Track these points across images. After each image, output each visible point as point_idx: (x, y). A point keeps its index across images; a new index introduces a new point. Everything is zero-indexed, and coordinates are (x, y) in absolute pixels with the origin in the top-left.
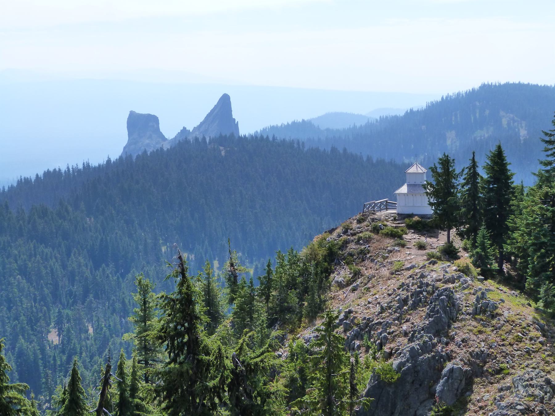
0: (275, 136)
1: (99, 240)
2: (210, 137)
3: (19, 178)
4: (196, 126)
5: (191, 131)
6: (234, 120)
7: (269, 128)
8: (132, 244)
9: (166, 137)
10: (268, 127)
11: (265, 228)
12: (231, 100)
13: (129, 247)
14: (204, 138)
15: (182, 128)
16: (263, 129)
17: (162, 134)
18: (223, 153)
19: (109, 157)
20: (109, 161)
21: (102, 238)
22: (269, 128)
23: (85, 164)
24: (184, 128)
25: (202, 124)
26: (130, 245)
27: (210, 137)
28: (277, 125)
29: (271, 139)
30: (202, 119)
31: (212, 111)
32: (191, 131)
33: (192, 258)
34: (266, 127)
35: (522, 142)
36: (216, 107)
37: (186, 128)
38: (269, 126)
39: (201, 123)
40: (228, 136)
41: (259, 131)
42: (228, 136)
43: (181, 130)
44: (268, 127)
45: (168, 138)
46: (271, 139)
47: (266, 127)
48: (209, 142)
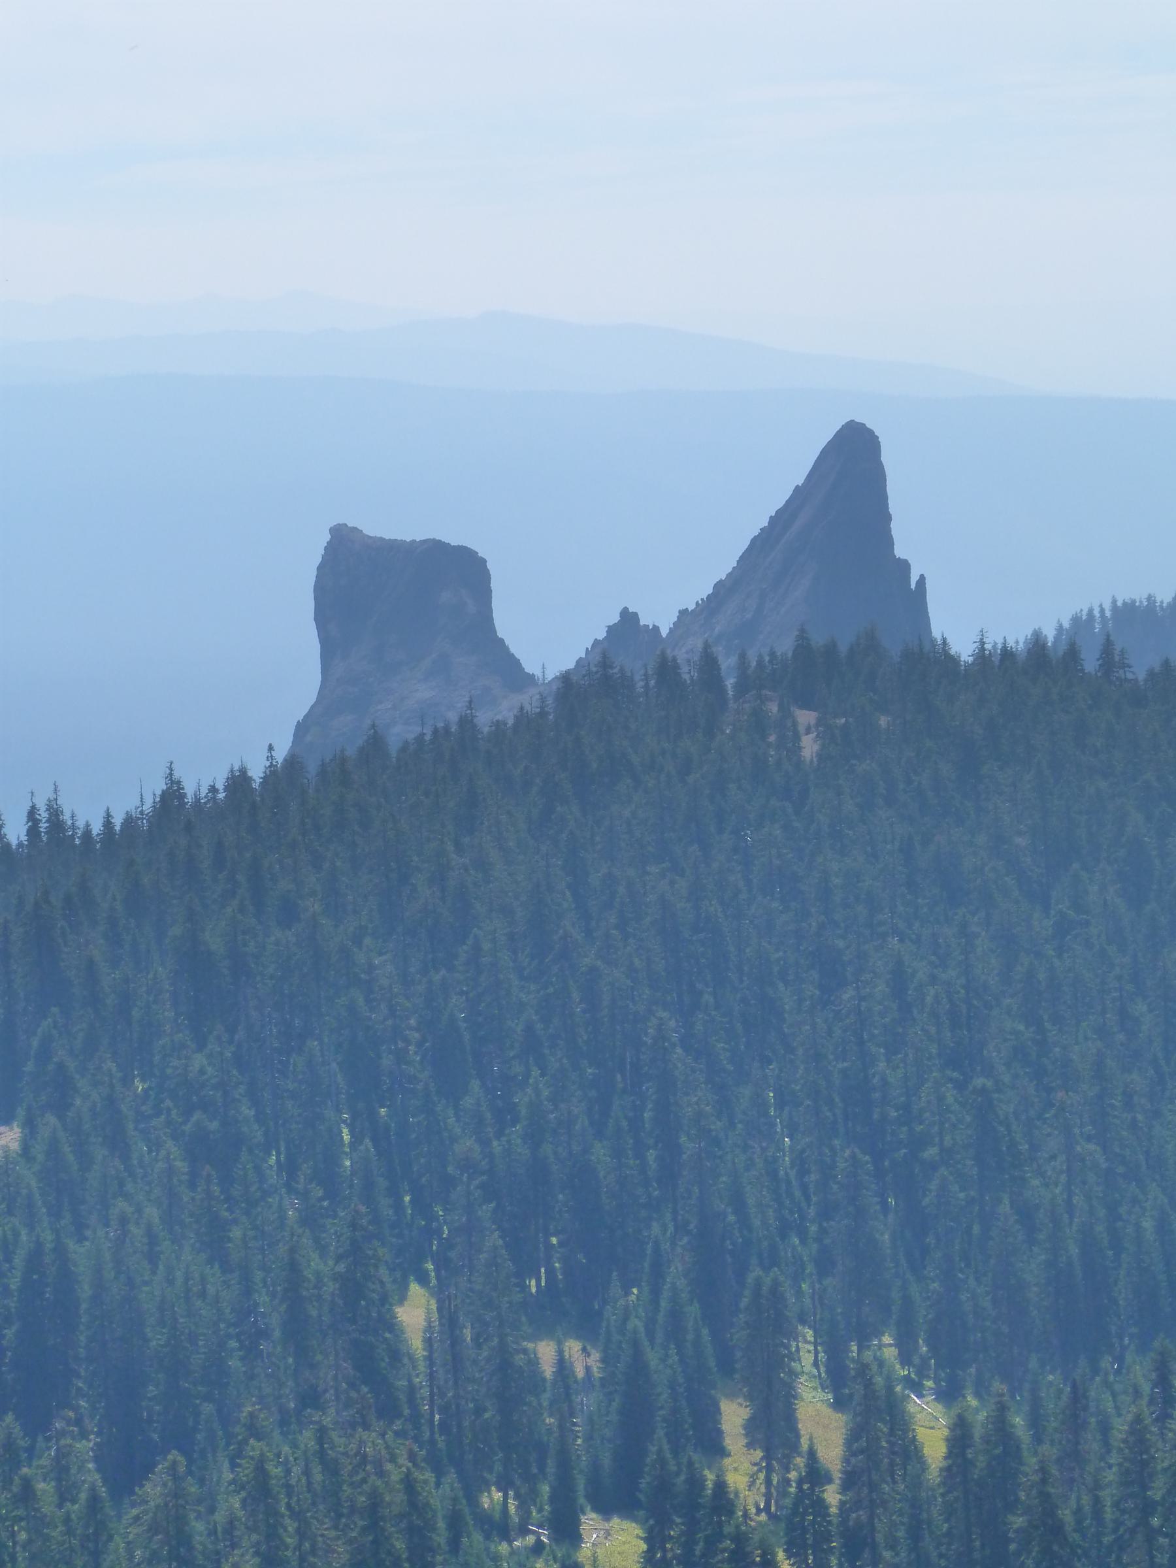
0: (1118, 648)
1: (19, 1261)
2: (743, 656)
3: (1074, 613)
4: (691, 607)
5: (664, 632)
6: (904, 566)
7: (1108, 614)
8: (211, 1290)
9: (531, 666)
10: (1102, 611)
11: (1036, 1182)
12: (889, 458)
13: (199, 1303)
14: (709, 663)
15: (615, 618)
16: (1076, 620)
17: (507, 648)
18: (809, 747)
19: (177, 775)
20: (172, 795)
21: (37, 1252)
22: (1108, 614)
23: (43, 815)
24: (628, 618)
25: (722, 592)
26: (203, 1294)
27: (743, 656)
28: (1149, 598)
29: (1090, 663)
30: (723, 565)
31: (781, 521)
32: (664, 632)
33: (588, 1369)
34: (1091, 611)
35: (792, 1400)
36: (800, 495)
37: (636, 615)
38: (1107, 607)
39: (718, 586)
40: (843, 648)
41: (1050, 634)
42: (843, 648)
43: (611, 629)
44: (1102, 611)
45: (538, 672)
46: (1090, 663)
47: (1091, 611)
48: (736, 686)
